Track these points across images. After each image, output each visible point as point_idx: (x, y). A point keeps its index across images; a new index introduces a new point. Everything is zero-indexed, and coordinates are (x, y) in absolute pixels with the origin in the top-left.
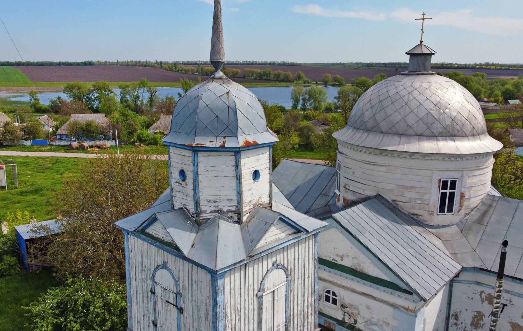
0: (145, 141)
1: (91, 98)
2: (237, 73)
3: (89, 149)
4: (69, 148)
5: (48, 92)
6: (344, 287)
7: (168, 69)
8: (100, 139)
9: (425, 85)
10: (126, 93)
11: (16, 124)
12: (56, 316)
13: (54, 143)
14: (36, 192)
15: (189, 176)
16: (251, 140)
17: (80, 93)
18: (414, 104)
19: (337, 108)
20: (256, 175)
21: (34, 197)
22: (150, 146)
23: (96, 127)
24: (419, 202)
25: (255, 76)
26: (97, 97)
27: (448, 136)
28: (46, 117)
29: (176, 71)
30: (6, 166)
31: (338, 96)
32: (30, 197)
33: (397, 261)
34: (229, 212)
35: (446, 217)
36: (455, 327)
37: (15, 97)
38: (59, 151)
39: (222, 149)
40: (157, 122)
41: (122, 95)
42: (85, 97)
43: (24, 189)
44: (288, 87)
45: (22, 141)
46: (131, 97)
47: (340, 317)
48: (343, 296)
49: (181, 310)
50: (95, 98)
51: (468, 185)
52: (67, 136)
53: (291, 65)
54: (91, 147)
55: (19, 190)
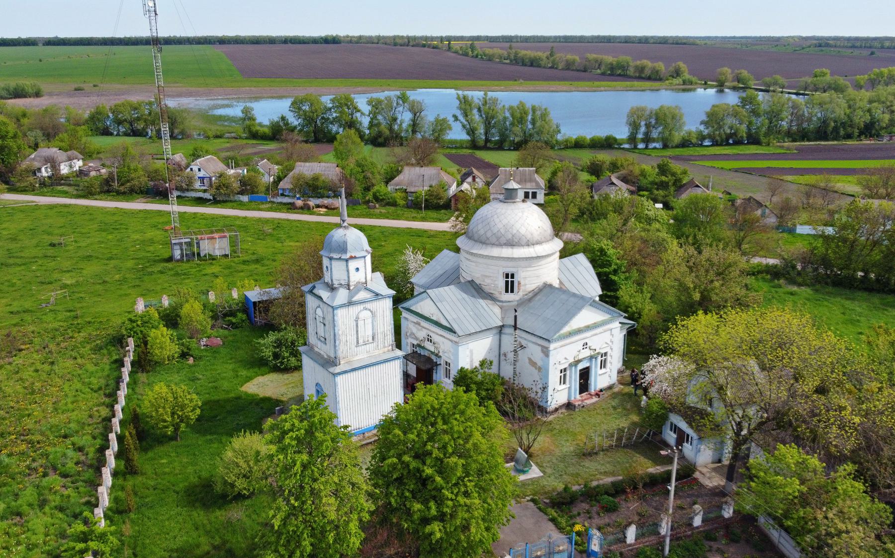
0: (383, 200)
1: (328, 118)
2: (574, 62)
3: (315, 210)
4: (291, 207)
5: (268, 97)
6: (434, 332)
7: (461, 52)
8: (328, 197)
12: (275, 347)
13: (275, 200)
14: (257, 261)
15: (329, 268)
18: (492, 224)
19: (702, 138)
20: (357, 269)
21: (256, 266)
23: (323, 181)
25: (603, 67)
29: (473, 57)
31: (704, 118)
32: (253, 267)
33: (455, 316)
35: (509, 296)
36: (505, 362)
38: (280, 211)
39: (340, 259)
43: (246, 258)
48: (435, 338)
49: (324, 325)
52: (291, 190)
53: (677, 44)
54: (318, 206)
55: (241, 258)
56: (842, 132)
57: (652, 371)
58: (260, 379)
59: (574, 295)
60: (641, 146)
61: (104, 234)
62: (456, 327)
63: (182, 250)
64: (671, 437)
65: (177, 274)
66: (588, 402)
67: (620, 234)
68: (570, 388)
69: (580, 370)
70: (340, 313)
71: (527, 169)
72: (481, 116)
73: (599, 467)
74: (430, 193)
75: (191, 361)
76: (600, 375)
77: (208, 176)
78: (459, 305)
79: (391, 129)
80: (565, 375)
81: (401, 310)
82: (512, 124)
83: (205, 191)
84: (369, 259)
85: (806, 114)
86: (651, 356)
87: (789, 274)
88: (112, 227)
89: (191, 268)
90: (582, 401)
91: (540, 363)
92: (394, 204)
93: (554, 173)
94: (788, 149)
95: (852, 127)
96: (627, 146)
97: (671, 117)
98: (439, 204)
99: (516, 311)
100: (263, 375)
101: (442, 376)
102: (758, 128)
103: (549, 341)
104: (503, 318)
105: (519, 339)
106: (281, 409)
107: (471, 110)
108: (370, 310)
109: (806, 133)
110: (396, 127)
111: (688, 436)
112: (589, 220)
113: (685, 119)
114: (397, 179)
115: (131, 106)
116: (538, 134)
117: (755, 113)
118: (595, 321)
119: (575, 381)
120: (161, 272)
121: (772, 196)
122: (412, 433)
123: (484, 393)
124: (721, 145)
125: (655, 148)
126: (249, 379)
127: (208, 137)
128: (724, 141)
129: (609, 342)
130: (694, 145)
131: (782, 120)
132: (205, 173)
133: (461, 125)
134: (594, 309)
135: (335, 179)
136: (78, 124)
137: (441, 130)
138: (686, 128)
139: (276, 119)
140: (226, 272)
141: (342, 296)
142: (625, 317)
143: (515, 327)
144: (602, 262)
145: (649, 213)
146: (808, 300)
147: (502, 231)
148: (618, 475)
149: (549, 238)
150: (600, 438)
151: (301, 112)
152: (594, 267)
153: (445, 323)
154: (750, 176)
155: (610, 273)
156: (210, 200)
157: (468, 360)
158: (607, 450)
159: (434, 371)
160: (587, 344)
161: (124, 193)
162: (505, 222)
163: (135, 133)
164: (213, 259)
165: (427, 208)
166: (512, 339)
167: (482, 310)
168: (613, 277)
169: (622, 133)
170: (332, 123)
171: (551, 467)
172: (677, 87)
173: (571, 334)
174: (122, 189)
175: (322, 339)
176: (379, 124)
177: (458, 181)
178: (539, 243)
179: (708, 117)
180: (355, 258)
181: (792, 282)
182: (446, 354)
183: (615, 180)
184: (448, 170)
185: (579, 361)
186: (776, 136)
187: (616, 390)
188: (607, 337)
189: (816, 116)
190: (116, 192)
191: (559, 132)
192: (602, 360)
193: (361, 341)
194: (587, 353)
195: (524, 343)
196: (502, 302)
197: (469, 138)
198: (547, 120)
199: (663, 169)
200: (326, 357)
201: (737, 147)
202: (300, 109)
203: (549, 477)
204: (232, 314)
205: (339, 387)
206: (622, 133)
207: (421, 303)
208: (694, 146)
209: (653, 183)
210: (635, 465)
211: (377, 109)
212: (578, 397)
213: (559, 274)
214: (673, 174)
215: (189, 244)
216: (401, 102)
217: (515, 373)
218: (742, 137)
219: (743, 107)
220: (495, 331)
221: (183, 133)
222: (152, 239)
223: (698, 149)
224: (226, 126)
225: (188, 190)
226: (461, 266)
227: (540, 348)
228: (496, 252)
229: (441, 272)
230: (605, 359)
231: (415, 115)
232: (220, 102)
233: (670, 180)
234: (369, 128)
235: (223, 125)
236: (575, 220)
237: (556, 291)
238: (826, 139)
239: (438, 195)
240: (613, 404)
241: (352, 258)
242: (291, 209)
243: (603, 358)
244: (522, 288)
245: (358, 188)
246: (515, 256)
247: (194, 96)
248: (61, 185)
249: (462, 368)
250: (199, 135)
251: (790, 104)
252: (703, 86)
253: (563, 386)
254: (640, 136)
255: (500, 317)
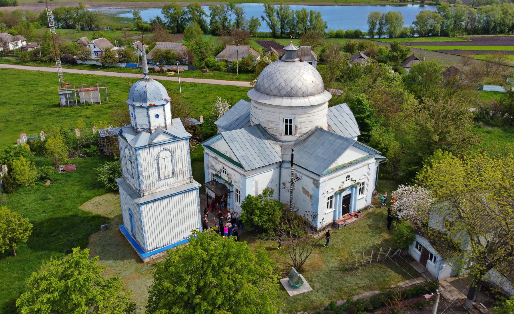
0: (212, 66)
1: (186, 18)
3: (167, 73)
5: (153, 7)
6: (227, 166)
9: (284, 68)
10: (216, 15)
11: (115, 48)
15: (133, 114)
16: (153, 104)
17: (175, 14)
18: (275, 78)
19: (413, 32)
20: (157, 116)
22: (215, 71)
23: (173, 54)
24: (275, 129)
26: (190, 17)
27: (289, 97)
28: (139, 42)
30: (100, 89)
31: (416, 20)
33: (244, 154)
34: (147, 129)
35: (288, 137)
36: (284, 189)
37: (123, 13)
40: (223, 51)
41: (211, 16)
42: (180, 18)
44: (384, 5)
45: (119, 63)
46: (220, 18)
47: (227, 180)
48: (229, 171)
50: (189, 18)
51: (298, 122)
54: (169, 71)
56: (498, 29)
57: (400, 198)
58: (97, 199)
59: (340, 137)
60: (376, 37)
61: (21, 87)
62: (243, 163)
63: (66, 98)
64: (417, 254)
65: (61, 116)
66: (349, 221)
67: (370, 89)
68: (335, 211)
69: (344, 197)
70: (142, 154)
71: (306, 47)
72: (279, 17)
73: (358, 282)
74: (242, 63)
75: (48, 183)
76: (358, 200)
77: (100, 51)
78: (247, 144)
79: (223, 25)
80: (331, 202)
81: (204, 147)
82: (298, 22)
83: (97, 61)
84: (168, 107)
85: (477, 18)
86: (399, 186)
87: (484, 118)
88: (28, 83)
89: (72, 111)
90: (344, 221)
91: (311, 192)
92: (219, 69)
93: (323, 51)
94: (466, 39)
95: (505, 26)
96: (367, 37)
97: (395, 18)
98: (248, 69)
99: (293, 150)
100: (100, 195)
101: (234, 201)
102: (448, 26)
103: (319, 176)
104: (282, 155)
105: (295, 172)
106: (105, 226)
107: (273, 13)
108: (169, 150)
109: (476, 30)
110: (227, 24)
111: (432, 255)
112: (348, 79)
113: (403, 20)
114: (221, 53)
115: (65, 10)
116: (313, 28)
117: (446, 17)
118: (357, 158)
119: (339, 206)
120: (50, 114)
121: (464, 66)
122: (181, 286)
123: (266, 217)
124: (425, 37)
125: (384, 38)
126: (88, 199)
127: (113, 30)
128: (427, 35)
129: (366, 174)
130: (408, 36)
131: (462, 22)
132: (98, 49)
133: (266, 22)
134: (356, 149)
135: (181, 53)
136: (33, 21)
137: (254, 26)
138: (405, 26)
139: (154, 19)
140: (96, 114)
141: (144, 138)
142: (380, 154)
143: (292, 163)
144: (359, 110)
145: (389, 75)
146: (500, 137)
147: (283, 84)
148: (375, 290)
149: (320, 90)
150: (359, 254)
151: (169, 14)
152: (354, 113)
153: (235, 159)
154: (445, 55)
155: (364, 118)
156: (101, 66)
157: (254, 189)
158: (365, 265)
159: (228, 197)
160: (349, 176)
161: (45, 61)
162: (285, 77)
163: (68, 27)
164: (89, 105)
165: (240, 72)
166: (289, 172)
167: (266, 149)
168: (367, 121)
169: (365, 29)
170: (187, 21)
171: (319, 282)
172: (396, 3)
173: (337, 169)
174: (44, 59)
175: (130, 174)
176: (216, 22)
177: (261, 55)
178: (312, 94)
179: (417, 19)
180: (154, 106)
181: (488, 124)
182: (236, 184)
183: (362, 55)
184: (257, 49)
185: (343, 190)
186: (459, 31)
187: (371, 210)
188: (365, 170)
189: (483, 19)
190: (41, 61)
191: (326, 27)
192: (360, 188)
193: (162, 176)
194: (349, 183)
195: (299, 175)
196: (282, 142)
197: (272, 31)
198: (319, 19)
199: (394, 48)
200: (134, 188)
201: (435, 38)
202: (168, 12)
203: (317, 291)
204: (88, 146)
205: (144, 214)
206: (365, 29)
207: (218, 143)
208: (408, 37)
209: (388, 57)
210: (388, 279)
211: (215, 12)
212: (341, 218)
213: (328, 119)
214: (401, 51)
215: (72, 94)
216: (230, 8)
217: (291, 199)
218: (438, 32)
219: (439, 13)
220: (276, 166)
221: (97, 27)
222: (52, 91)
223: (411, 39)
224: (125, 23)
225: (86, 60)
226: (251, 112)
227: (312, 181)
228: (278, 101)
229: (237, 117)
230: (363, 187)
231: (238, 16)
232: (124, 10)
233: (399, 55)
234: (210, 25)
235: (122, 23)
236: (338, 80)
237: (326, 133)
238: (489, 34)
239: (247, 64)
240: (369, 223)
241: (151, 106)
242: (151, 72)
243: (362, 186)
244: (298, 131)
245: (196, 59)
246: (293, 105)
247: (109, 6)
248: (7, 56)
249: (249, 195)
250: (107, 28)
251: (468, 12)
252: (412, 3)
253: (330, 210)
254: (376, 31)
255: (280, 154)
